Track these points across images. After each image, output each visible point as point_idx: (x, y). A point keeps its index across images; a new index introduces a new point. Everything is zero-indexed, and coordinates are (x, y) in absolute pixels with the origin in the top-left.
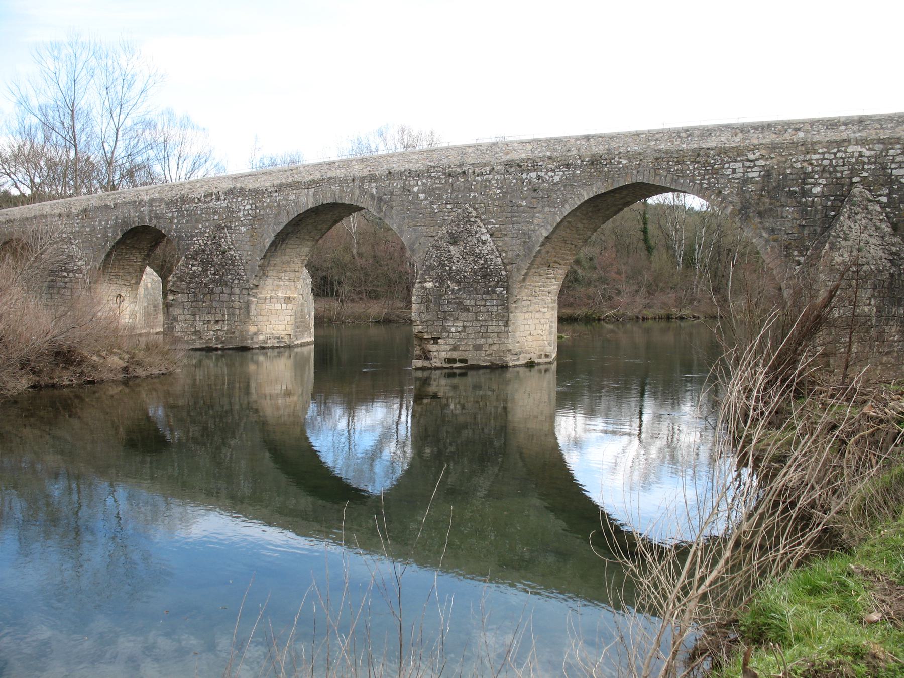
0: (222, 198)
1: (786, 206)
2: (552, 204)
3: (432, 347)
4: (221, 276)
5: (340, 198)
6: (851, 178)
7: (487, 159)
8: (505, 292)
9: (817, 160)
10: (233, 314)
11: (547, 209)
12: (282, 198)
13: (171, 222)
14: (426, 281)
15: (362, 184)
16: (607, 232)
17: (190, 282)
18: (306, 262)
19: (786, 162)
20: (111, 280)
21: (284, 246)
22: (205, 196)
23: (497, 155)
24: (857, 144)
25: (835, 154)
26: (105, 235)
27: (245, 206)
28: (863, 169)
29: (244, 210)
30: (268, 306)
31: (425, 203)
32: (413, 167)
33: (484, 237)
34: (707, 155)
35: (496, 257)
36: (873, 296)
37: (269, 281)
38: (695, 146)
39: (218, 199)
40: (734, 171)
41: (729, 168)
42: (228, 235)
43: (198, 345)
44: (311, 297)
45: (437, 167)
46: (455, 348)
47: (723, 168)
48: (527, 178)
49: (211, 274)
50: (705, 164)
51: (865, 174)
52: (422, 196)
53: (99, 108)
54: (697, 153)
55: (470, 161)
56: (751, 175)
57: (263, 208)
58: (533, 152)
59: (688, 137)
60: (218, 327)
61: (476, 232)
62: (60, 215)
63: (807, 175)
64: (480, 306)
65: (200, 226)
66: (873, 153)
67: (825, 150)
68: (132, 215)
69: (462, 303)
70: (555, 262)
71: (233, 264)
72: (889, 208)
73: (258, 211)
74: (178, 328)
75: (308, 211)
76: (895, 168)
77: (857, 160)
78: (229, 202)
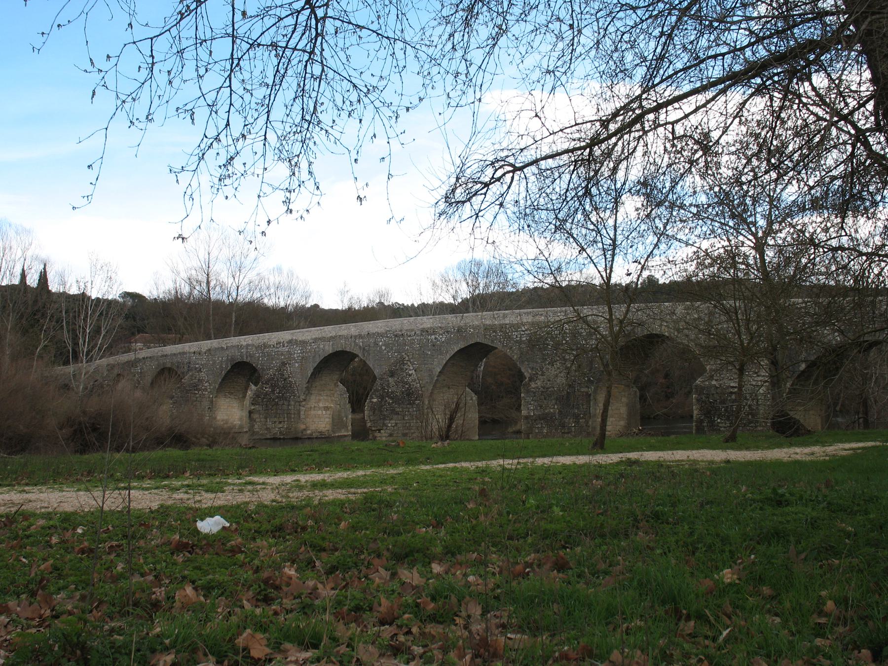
2: (441, 354)
3: (377, 434)
4: (283, 394)
5: (345, 348)
7: (413, 328)
10: (291, 418)
11: (439, 356)
13: (259, 359)
14: (373, 398)
17: (264, 398)
20: (225, 395)
21: (320, 375)
26: (221, 366)
30: (313, 412)
33: (410, 372)
34: (506, 327)
36: (556, 403)
37: (313, 397)
39: (284, 346)
43: (268, 436)
44: (348, 406)
46: (391, 435)
53: (226, 272)
55: (405, 328)
57: (307, 352)
60: (281, 426)
62: (194, 353)
71: (290, 386)
74: (256, 426)
75: (329, 355)
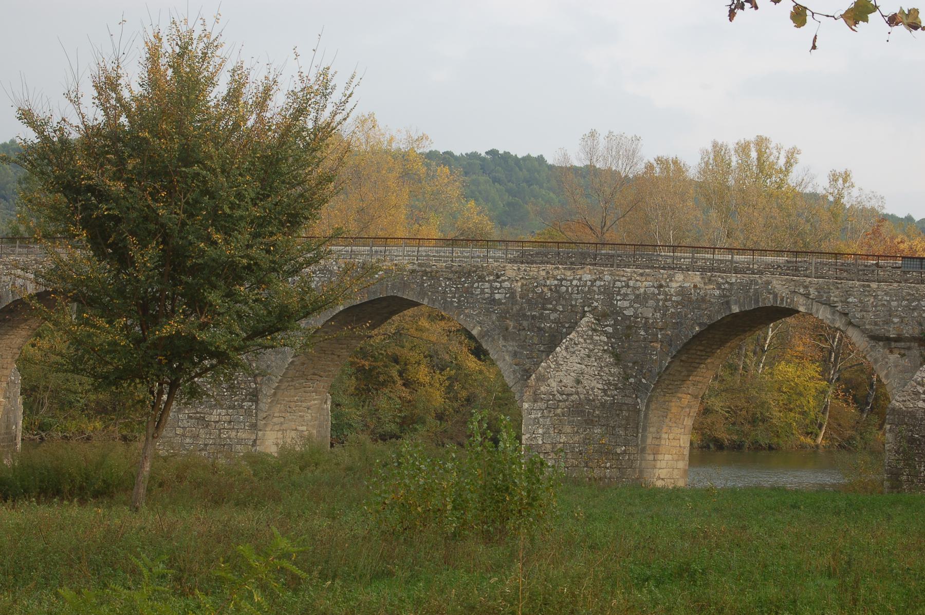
8: (254, 407)
16: (407, 319)
18: (17, 357)
47: (472, 287)
51: (595, 304)
56: (497, 296)
69: (204, 417)
70: (314, 374)
72: (614, 338)
76: (620, 300)
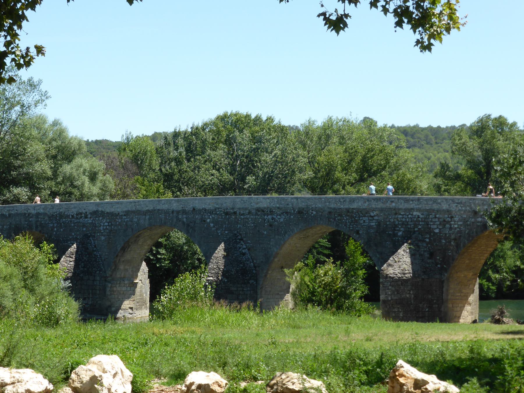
0: (89, 216)
1: (387, 241)
6: (414, 228)
8: (255, 283)
9: (400, 218)
11: (277, 237)
12: (128, 220)
13: (53, 230)
15: (178, 215)
19: (387, 218)
22: (77, 215)
23: (252, 204)
24: (417, 211)
25: (408, 215)
27: (104, 224)
28: (419, 224)
29: (104, 226)
31: (213, 229)
32: (207, 207)
34: (352, 212)
35: (251, 263)
38: (347, 207)
39: (86, 217)
40: (364, 221)
41: (362, 220)
42: (92, 241)
45: (221, 208)
47: (359, 220)
48: (267, 219)
49: (82, 267)
50: (352, 217)
51: (420, 227)
52: (212, 225)
54: (348, 210)
56: (372, 224)
58: (270, 204)
59: (344, 202)
61: (240, 248)
63: (396, 226)
64: (240, 291)
65: (73, 234)
66: (423, 216)
67: (404, 213)
68: (23, 223)
73: (113, 227)
76: (432, 225)
77: (417, 219)
78: (93, 220)
